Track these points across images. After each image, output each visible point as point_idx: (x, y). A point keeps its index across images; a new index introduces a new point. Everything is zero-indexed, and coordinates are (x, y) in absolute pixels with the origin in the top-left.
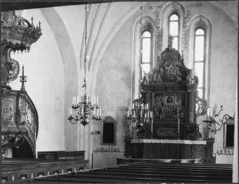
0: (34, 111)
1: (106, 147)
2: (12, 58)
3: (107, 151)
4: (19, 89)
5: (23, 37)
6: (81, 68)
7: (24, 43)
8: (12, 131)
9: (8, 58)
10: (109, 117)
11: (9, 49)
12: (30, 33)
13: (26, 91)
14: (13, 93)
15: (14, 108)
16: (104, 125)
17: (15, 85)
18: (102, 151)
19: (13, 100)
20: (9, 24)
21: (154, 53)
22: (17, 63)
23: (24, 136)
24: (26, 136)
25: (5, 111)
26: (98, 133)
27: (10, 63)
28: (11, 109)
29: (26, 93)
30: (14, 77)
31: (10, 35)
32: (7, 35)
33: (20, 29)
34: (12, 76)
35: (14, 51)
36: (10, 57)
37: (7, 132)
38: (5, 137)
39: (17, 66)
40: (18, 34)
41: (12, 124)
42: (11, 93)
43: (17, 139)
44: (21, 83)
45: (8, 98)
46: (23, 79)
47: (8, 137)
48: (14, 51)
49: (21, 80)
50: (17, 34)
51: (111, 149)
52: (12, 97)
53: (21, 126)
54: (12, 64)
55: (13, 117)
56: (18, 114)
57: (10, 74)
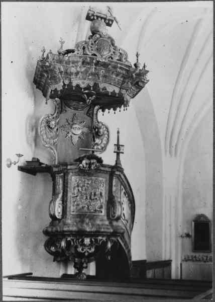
0: (132, 199)
1: (199, 255)
2: (99, 121)
3: (200, 260)
4: (113, 164)
5: (124, 82)
6: (166, 154)
7: (124, 91)
8: (102, 230)
9: (95, 120)
10: (203, 215)
11: (97, 107)
12: (134, 75)
13: (123, 167)
14: (107, 169)
15: (105, 193)
16: (195, 226)
17: (108, 158)
18: (194, 259)
19: (104, 180)
20: (105, 59)
21: (124, 180)
22: (107, 128)
23: (119, 239)
24: (121, 239)
25: (92, 197)
26: (188, 235)
27: (97, 128)
28: (101, 194)
29: (122, 171)
30: (102, 148)
31: (105, 76)
32: (100, 76)
33: (121, 68)
34: (99, 147)
35: (103, 111)
36: (97, 117)
37: (96, 232)
38: (91, 241)
39: (106, 132)
40: (117, 75)
41: (102, 220)
42: (102, 168)
43: (109, 245)
44: (116, 154)
45: (98, 177)
46: (118, 149)
47: (96, 240)
48: (103, 111)
49: (116, 151)
50: (114, 76)
51: (205, 258)
52: (104, 175)
53: (115, 223)
54: (100, 128)
55: (104, 207)
56: (111, 202)
57: (97, 144)
